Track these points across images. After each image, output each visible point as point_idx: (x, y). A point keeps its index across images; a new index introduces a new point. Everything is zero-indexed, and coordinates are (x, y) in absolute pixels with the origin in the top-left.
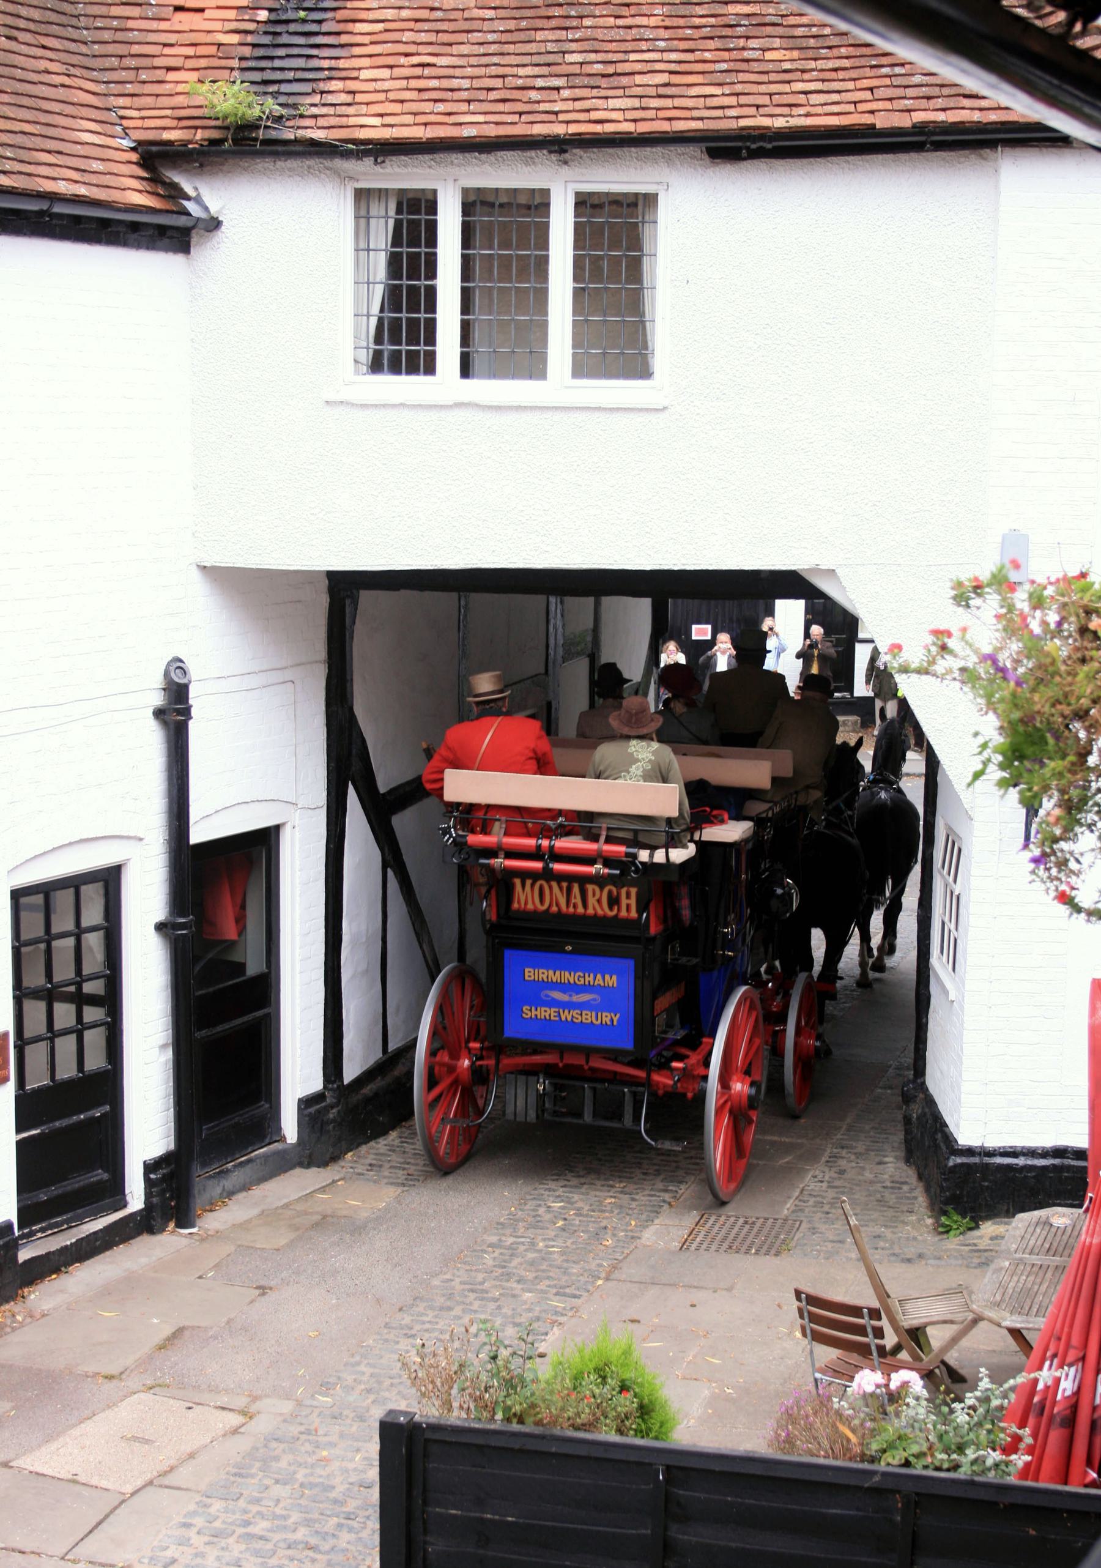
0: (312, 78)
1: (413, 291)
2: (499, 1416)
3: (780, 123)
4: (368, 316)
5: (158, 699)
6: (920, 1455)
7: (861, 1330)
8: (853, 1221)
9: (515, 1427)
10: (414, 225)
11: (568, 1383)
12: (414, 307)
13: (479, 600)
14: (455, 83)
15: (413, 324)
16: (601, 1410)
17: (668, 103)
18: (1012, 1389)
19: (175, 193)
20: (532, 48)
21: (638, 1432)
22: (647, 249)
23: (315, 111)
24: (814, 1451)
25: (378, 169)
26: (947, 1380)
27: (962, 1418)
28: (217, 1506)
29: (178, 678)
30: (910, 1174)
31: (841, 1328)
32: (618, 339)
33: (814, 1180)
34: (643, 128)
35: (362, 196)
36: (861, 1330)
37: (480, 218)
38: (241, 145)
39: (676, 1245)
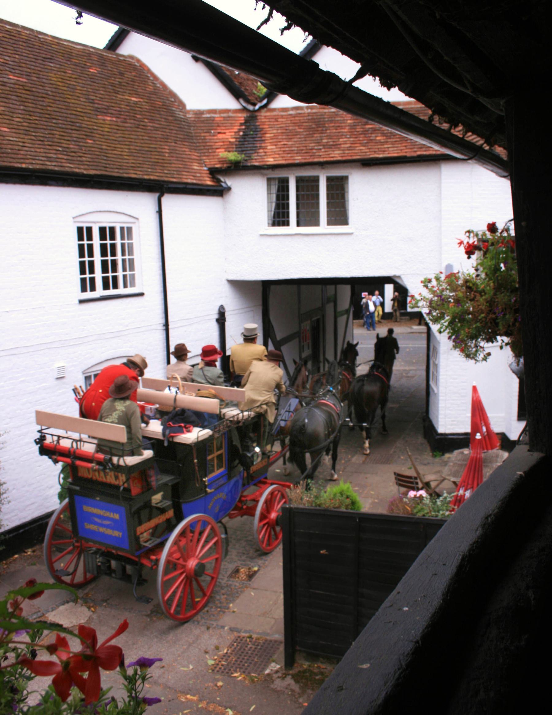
0: (255, 150)
1: (283, 204)
2: (314, 505)
3: (381, 156)
4: (271, 211)
5: (216, 316)
6: (427, 513)
7: (412, 483)
8: (410, 454)
9: (318, 508)
10: (283, 187)
11: (332, 496)
12: (283, 208)
13: (303, 287)
14: (293, 149)
15: (283, 213)
16: (341, 503)
17: (350, 152)
18: (453, 496)
19: (219, 181)
20: (313, 139)
21: (351, 509)
22: (346, 190)
23: (256, 158)
24: (399, 513)
25: (273, 172)
26: (435, 495)
27: (439, 503)
28: (238, 533)
29: (222, 311)
30: (425, 441)
31: (406, 482)
32: (339, 215)
33: (399, 444)
34: (344, 158)
35: (269, 180)
36: (412, 483)
37: (301, 184)
38: (236, 169)
39: (361, 462)
